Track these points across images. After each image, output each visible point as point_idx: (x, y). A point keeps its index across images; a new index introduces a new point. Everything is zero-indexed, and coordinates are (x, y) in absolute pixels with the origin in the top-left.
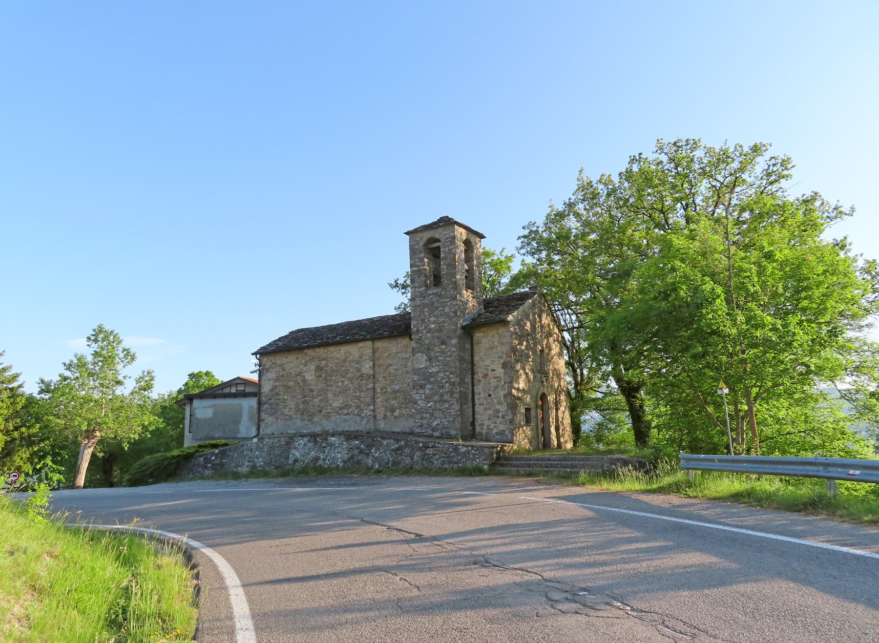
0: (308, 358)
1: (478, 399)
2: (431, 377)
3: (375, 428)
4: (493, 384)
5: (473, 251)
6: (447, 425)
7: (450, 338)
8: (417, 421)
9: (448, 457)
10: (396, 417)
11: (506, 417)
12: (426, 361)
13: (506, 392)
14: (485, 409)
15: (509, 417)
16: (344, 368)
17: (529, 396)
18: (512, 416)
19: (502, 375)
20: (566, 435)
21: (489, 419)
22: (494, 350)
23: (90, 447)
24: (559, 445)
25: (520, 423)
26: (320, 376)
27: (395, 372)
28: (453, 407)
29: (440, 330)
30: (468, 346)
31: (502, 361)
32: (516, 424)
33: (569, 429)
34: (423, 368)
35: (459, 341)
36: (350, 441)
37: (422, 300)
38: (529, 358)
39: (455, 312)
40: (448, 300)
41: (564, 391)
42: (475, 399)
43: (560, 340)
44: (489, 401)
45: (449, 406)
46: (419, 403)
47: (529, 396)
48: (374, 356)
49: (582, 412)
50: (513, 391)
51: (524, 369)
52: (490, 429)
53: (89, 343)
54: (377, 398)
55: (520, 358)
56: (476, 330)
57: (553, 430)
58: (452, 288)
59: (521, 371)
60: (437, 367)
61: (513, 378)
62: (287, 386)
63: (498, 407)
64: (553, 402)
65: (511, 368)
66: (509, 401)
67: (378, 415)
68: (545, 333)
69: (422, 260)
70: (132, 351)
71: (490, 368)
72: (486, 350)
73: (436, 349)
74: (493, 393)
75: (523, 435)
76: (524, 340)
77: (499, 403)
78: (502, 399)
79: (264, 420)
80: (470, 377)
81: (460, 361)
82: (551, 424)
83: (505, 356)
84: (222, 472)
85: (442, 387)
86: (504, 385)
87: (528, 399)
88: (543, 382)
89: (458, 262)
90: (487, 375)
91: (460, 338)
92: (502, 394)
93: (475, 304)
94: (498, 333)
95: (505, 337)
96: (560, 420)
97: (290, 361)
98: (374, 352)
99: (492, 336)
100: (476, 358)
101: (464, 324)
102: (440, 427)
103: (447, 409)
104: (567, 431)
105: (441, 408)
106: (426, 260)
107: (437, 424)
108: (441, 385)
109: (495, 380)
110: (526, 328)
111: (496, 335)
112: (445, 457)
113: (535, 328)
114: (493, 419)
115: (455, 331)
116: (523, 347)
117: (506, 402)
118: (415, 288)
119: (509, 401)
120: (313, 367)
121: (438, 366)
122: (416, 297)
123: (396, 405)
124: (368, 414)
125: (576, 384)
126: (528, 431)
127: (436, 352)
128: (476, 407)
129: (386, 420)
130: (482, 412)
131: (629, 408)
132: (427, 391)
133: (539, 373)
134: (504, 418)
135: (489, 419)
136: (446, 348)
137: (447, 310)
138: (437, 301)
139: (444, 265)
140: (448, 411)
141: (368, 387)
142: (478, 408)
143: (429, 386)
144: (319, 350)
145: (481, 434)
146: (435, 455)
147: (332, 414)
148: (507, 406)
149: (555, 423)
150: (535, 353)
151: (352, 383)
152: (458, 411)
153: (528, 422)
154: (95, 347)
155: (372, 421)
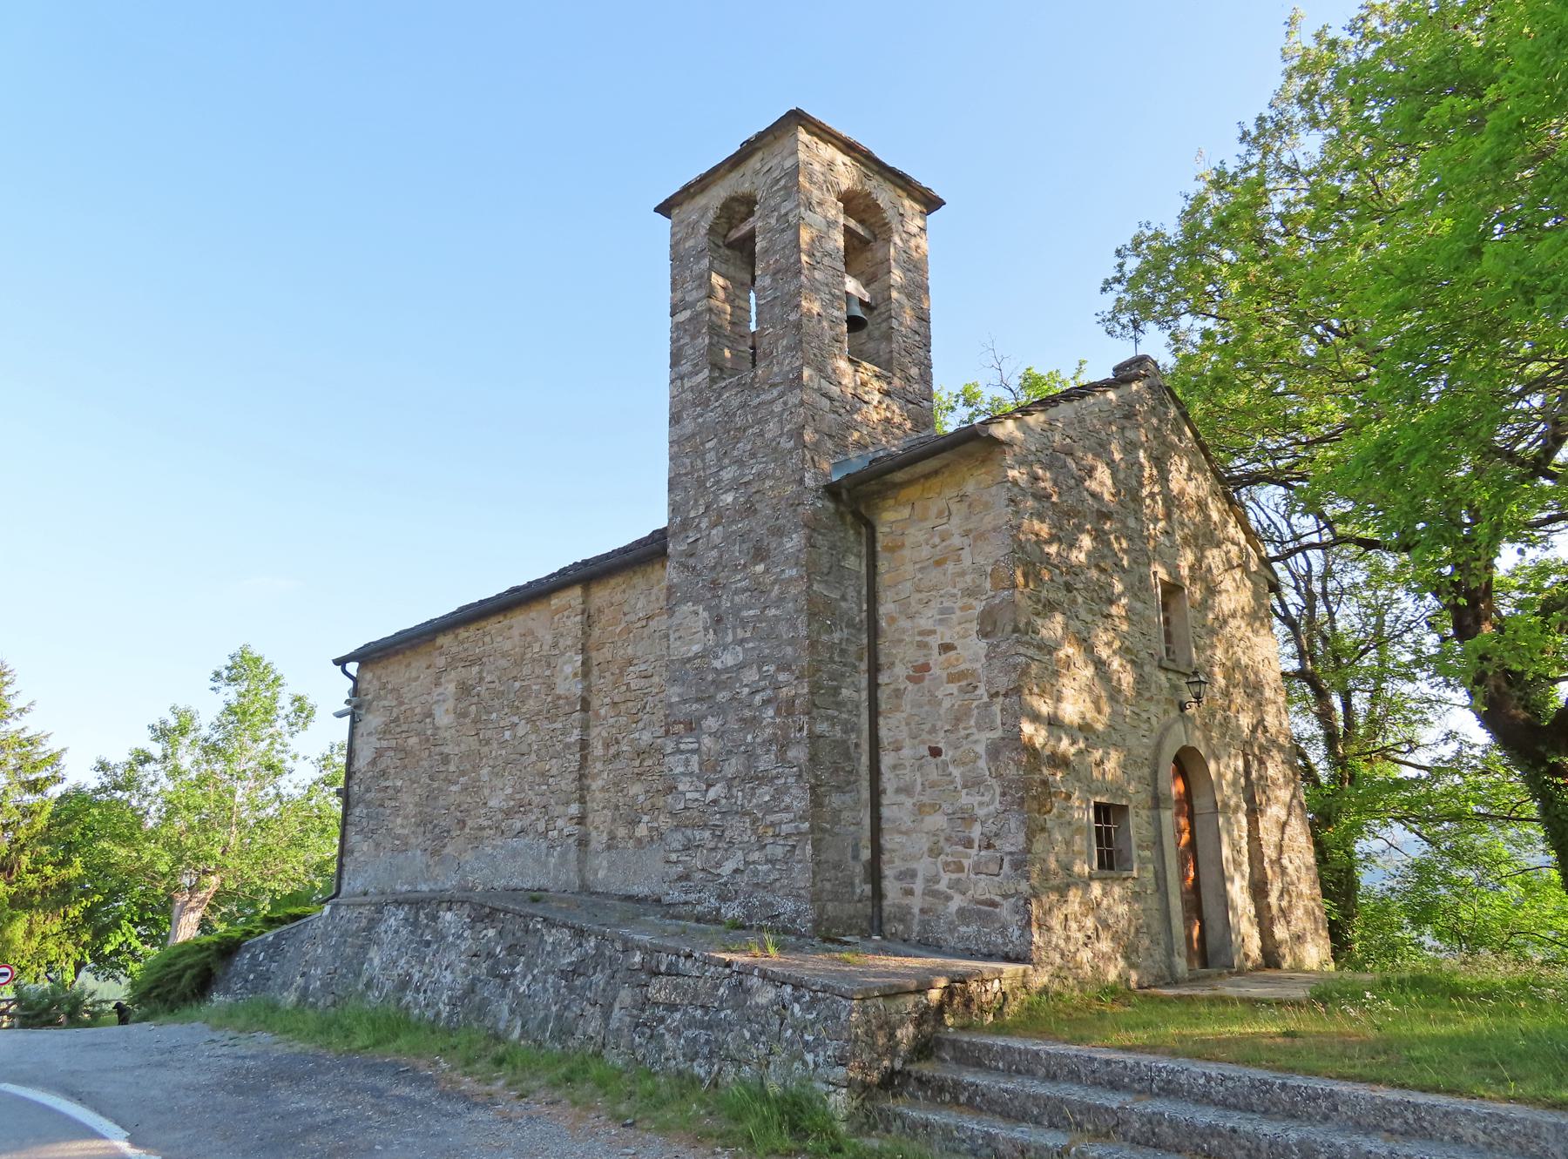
0: (441, 662)
1: (895, 767)
2: (718, 685)
3: (583, 880)
4: (946, 704)
5: (889, 240)
6: (767, 873)
7: (779, 532)
8: (674, 857)
9: (709, 1026)
10: (639, 841)
11: (997, 843)
12: (706, 629)
13: (998, 734)
14: (920, 809)
15: (1013, 842)
16: (517, 684)
17: (1114, 755)
18: (1021, 838)
20: (1299, 912)
21: (935, 852)
22: (950, 567)
23: (192, 909)
24: (1271, 957)
25: (1067, 868)
26: (464, 715)
27: (643, 682)
28: (787, 800)
29: (749, 510)
30: (855, 563)
31: (979, 606)
32: (1045, 872)
33: (1307, 886)
34: (696, 657)
35: (809, 538)
36: (479, 926)
38: (1111, 602)
39: (798, 434)
41: (1281, 748)
42: (883, 768)
43: (1253, 568)
44: (934, 775)
45: (773, 798)
46: (681, 787)
47: (1114, 755)
48: (586, 634)
49: (1357, 830)
50: (1028, 728)
51: (1087, 645)
52: (935, 894)
53: (216, 685)
54: (595, 777)
55: (1061, 595)
56: (884, 498)
57: (1238, 891)
58: (788, 348)
59: (1068, 650)
60: (739, 649)
61: (1025, 672)
62: (404, 750)
64: (1234, 783)
65: (1016, 630)
66: (1012, 771)
67: (594, 834)
68: (1182, 524)
69: (704, 281)
70: (310, 701)
71: (934, 641)
72: (922, 569)
73: (739, 581)
75: (1090, 922)
76: (1080, 528)
77: (974, 783)
78: (982, 764)
79: (352, 853)
81: (812, 615)
82: (1230, 869)
83: (988, 585)
84: (74, 1020)
85: (752, 723)
86: (987, 705)
87: (1111, 765)
88: (1182, 707)
89: (811, 255)
90: (925, 668)
91: (812, 526)
92: (983, 740)
93: (897, 419)
94: (962, 498)
95: (987, 507)
96: (1270, 852)
97: (414, 674)
98: (588, 620)
99: (940, 515)
100: (886, 608)
101: (835, 478)
102: (743, 881)
103: (768, 810)
104: (1300, 895)
105: (748, 806)
106: (717, 280)
107: (736, 871)
108: (748, 713)
109: (953, 688)
110: (1092, 485)
111: (954, 507)
112: (702, 1025)
113: (1137, 499)
114: (951, 851)
115: (795, 504)
116: (1078, 557)
117: (999, 776)
118: (682, 378)
119: (1012, 771)
120: (451, 687)
122: (684, 408)
123: (641, 798)
124: (566, 832)
125: (1331, 739)
126: (1115, 901)
127: (736, 592)
128: (885, 800)
130: (908, 823)
131: (1544, 810)
132: (707, 741)
133: (1161, 667)
134: (989, 846)
135: (935, 852)
136: (767, 571)
137: (772, 428)
138: (744, 405)
139: (764, 274)
140: (770, 818)
141: (568, 740)
142: (895, 809)
143: (711, 723)
145: (904, 915)
146: (672, 1007)
148: (1004, 794)
149: (1246, 868)
150: (1137, 588)
151: (536, 731)
152: (802, 819)
153: (1110, 860)
154: (230, 693)
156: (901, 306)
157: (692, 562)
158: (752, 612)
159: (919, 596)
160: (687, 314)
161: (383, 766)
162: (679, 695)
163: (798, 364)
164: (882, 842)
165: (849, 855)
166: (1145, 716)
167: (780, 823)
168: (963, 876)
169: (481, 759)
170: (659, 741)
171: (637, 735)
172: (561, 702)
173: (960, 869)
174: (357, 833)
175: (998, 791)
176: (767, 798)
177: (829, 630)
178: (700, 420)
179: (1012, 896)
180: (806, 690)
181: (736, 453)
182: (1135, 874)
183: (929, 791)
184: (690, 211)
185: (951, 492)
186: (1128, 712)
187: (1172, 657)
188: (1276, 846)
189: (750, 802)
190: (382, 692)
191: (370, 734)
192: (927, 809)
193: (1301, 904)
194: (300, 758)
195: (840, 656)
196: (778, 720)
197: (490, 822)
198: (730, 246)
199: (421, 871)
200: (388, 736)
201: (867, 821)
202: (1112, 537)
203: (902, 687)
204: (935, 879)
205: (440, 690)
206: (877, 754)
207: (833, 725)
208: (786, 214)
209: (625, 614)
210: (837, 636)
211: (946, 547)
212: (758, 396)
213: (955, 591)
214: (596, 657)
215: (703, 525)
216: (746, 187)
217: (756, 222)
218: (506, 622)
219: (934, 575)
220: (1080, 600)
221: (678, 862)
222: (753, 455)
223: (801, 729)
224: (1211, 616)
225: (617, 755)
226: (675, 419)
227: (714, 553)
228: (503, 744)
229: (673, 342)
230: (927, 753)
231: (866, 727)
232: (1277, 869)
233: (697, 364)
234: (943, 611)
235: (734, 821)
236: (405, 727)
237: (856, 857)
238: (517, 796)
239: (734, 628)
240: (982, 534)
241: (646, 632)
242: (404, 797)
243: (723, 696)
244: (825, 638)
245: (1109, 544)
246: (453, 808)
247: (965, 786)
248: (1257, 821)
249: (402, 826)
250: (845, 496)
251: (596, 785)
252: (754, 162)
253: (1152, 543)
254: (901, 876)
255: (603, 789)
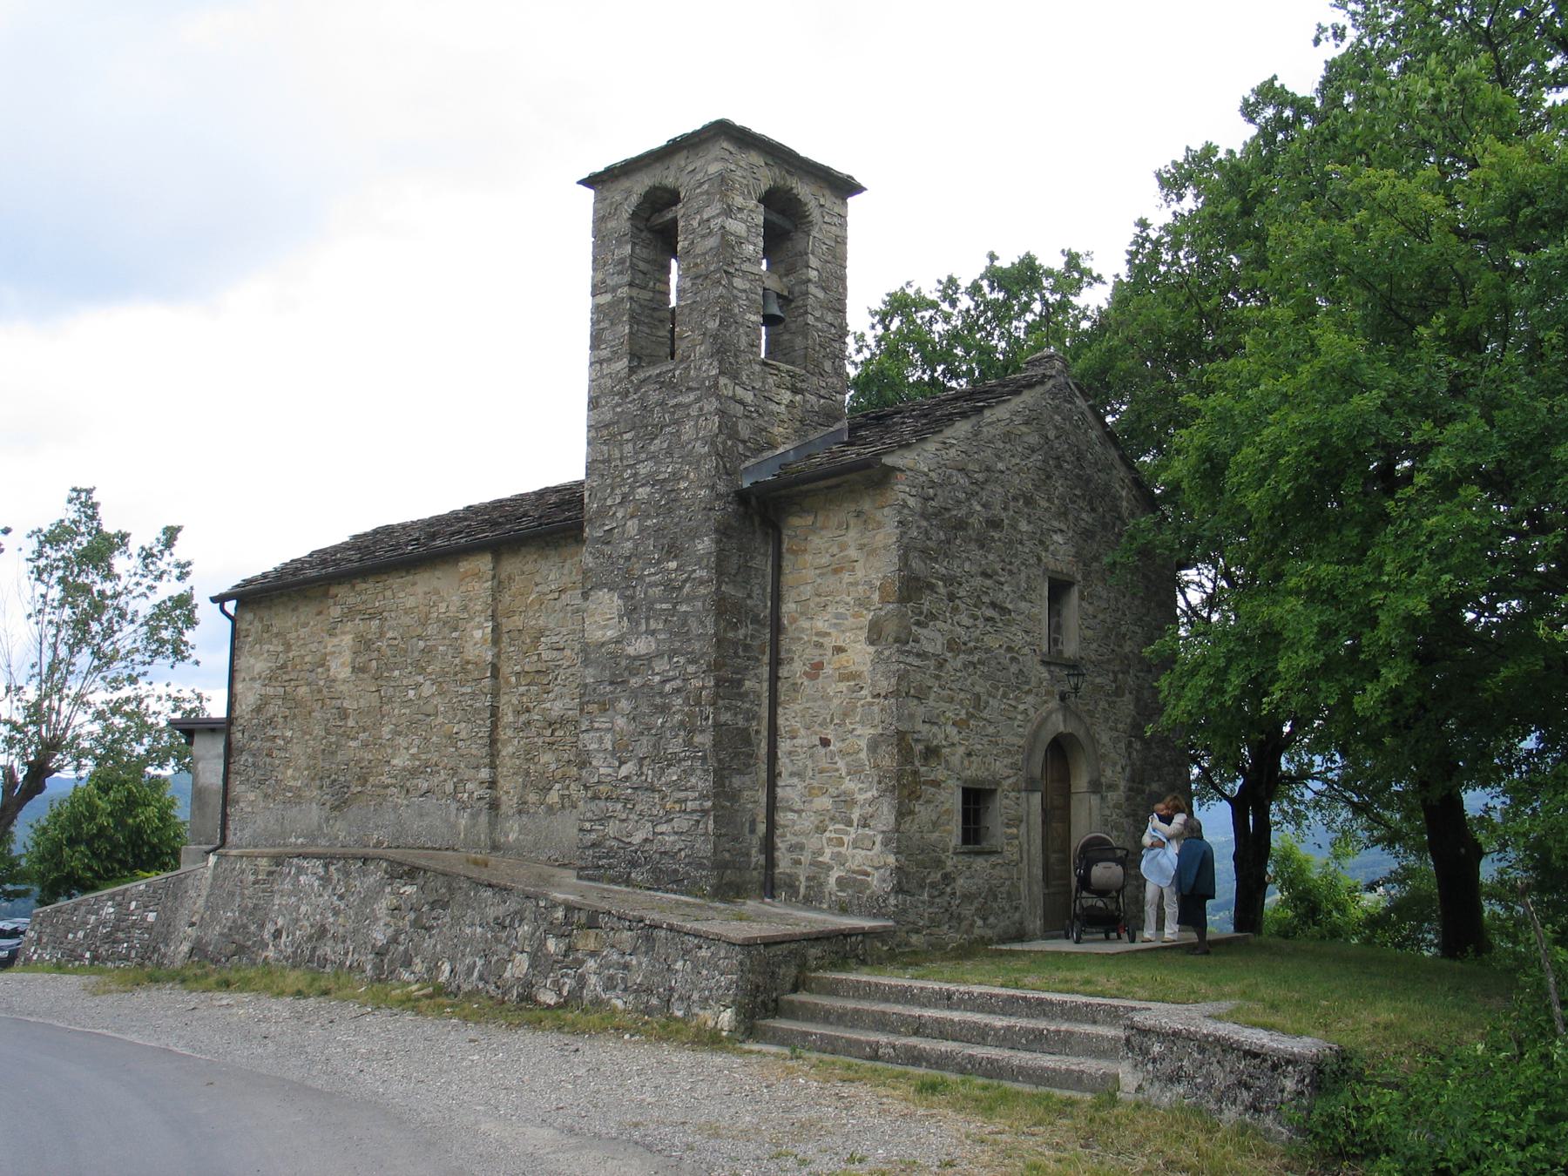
2: (633, 672)
6: (673, 843)
8: (588, 825)
10: (550, 808)
12: (621, 617)
16: (421, 644)
19: (866, 669)
22: (846, 577)
34: (610, 641)
37: (619, 405)
40: (692, 397)
46: (595, 763)
54: (505, 744)
63: (849, 785)
67: (504, 798)
74: (837, 736)
78: (863, 755)
79: (237, 802)
80: (765, 671)
83: (876, 597)
97: (303, 619)
100: (789, 607)
105: (657, 784)
107: (646, 840)
108: (658, 700)
109: (843, 686)
121: (653, 633)
127: (651, 585)
128: (780, 783)
129: (525, 818)
138: (662, 404)
142: (789, 790)
144: (364, 586)
147: (389, 791)
155: (483, 819)
157: (607, 549)
158: (664, 606)
159: (818, 599)
160: (607, 298)
161: (270, 714)
162: (594, 676)
163: (714, 373)
164: (776, 818)
165: (747, 831)
166: (1021, 707)
167: (686, 800)
168: (843, 850)
169: (383, 717)
170: (570, 712)
171: (548, 705)
172: (470, 666)
173: (841, 843)
174: (242, 783)
175: (876, 779)
176: (675, 778)
177: (735, 627)
178: (619, 410)
179: (880, 868)
180: (712, 683)
181: (652, 448)
183: (818, 776)
184: (616, 193)
185: (853, 507)
189: (659, 779)
190: (265, 635)
191: (253, 679)
192: (816, 791)
194: (164, 697)
195: (744, 651)
196: (686, 709)
197: (394, 781)
198: (650, 230)
199: (319, 825)
200: (274, 684)
201: (763, 799)
203: (799, 682)
204: (820, 852)
205: (335, 641)
206: (776, 741)
207: (736, 714)
208: (708, 220)
209: (537, 585)
210: (741, 632)
211: (843, 557)
212: (675, 397)
213: (848, 599)
214: (507, 624)
215: (619, 515)
216: (670, 181)
217: (679, 210)
218: (410, 578)
219: (831, 581)
220: (963, 606)
221: (591, 831)
222: (669, 453)
223: (707, 718)
225: (528, 723)
226: (593, 404)
227: (629, 544)
228: (407, 703)
229: (593, 324)
230: (818, 742)
231: (766, 715)
233: (615, 352)
234: (838, 616)
235: (642, 796)
236: (293, 675)
237: (753, 831)
238: (423, 756)
239: (647, 619)
240: (875, 550)
241: (558, 605)
242: (296, 749)
243: (635, 682)
244: (731, 635)
246: (352, 763)
247: (849, 774)
249: (295, 779)
250: (754, 501)
251: (507, 751)
252: (680, 160)
254: (792, 848)
255: (513, 756)
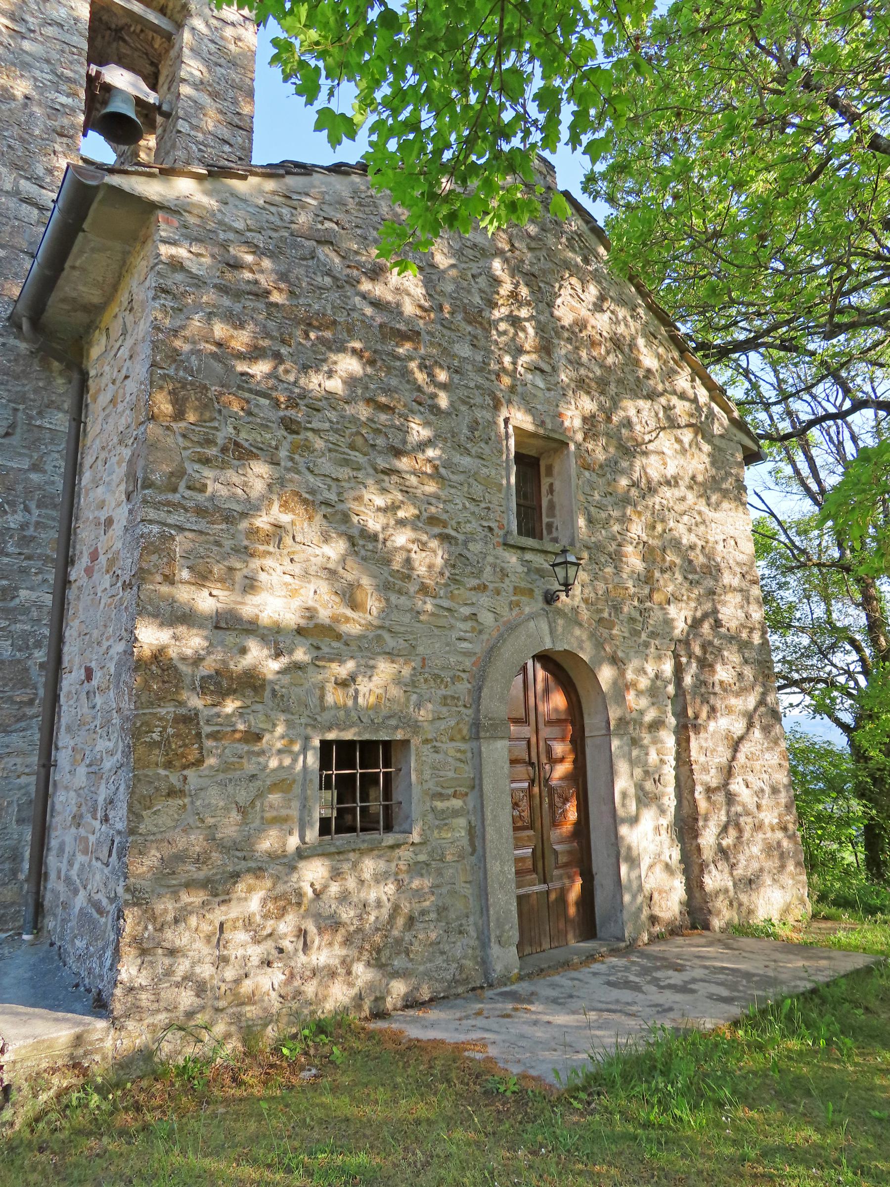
104: (758, 827)
156: (199, 107)
182: (415, 837)
186: (429, 607)
187: (555, 534)
188: (720, 769)
193: (760, 836)
202: (413, 365)
220: (319, 444)
224: (624, 482)
232: (720, 797)
245: (405, 374)
248: (688, 740)
253: (506, 380)
